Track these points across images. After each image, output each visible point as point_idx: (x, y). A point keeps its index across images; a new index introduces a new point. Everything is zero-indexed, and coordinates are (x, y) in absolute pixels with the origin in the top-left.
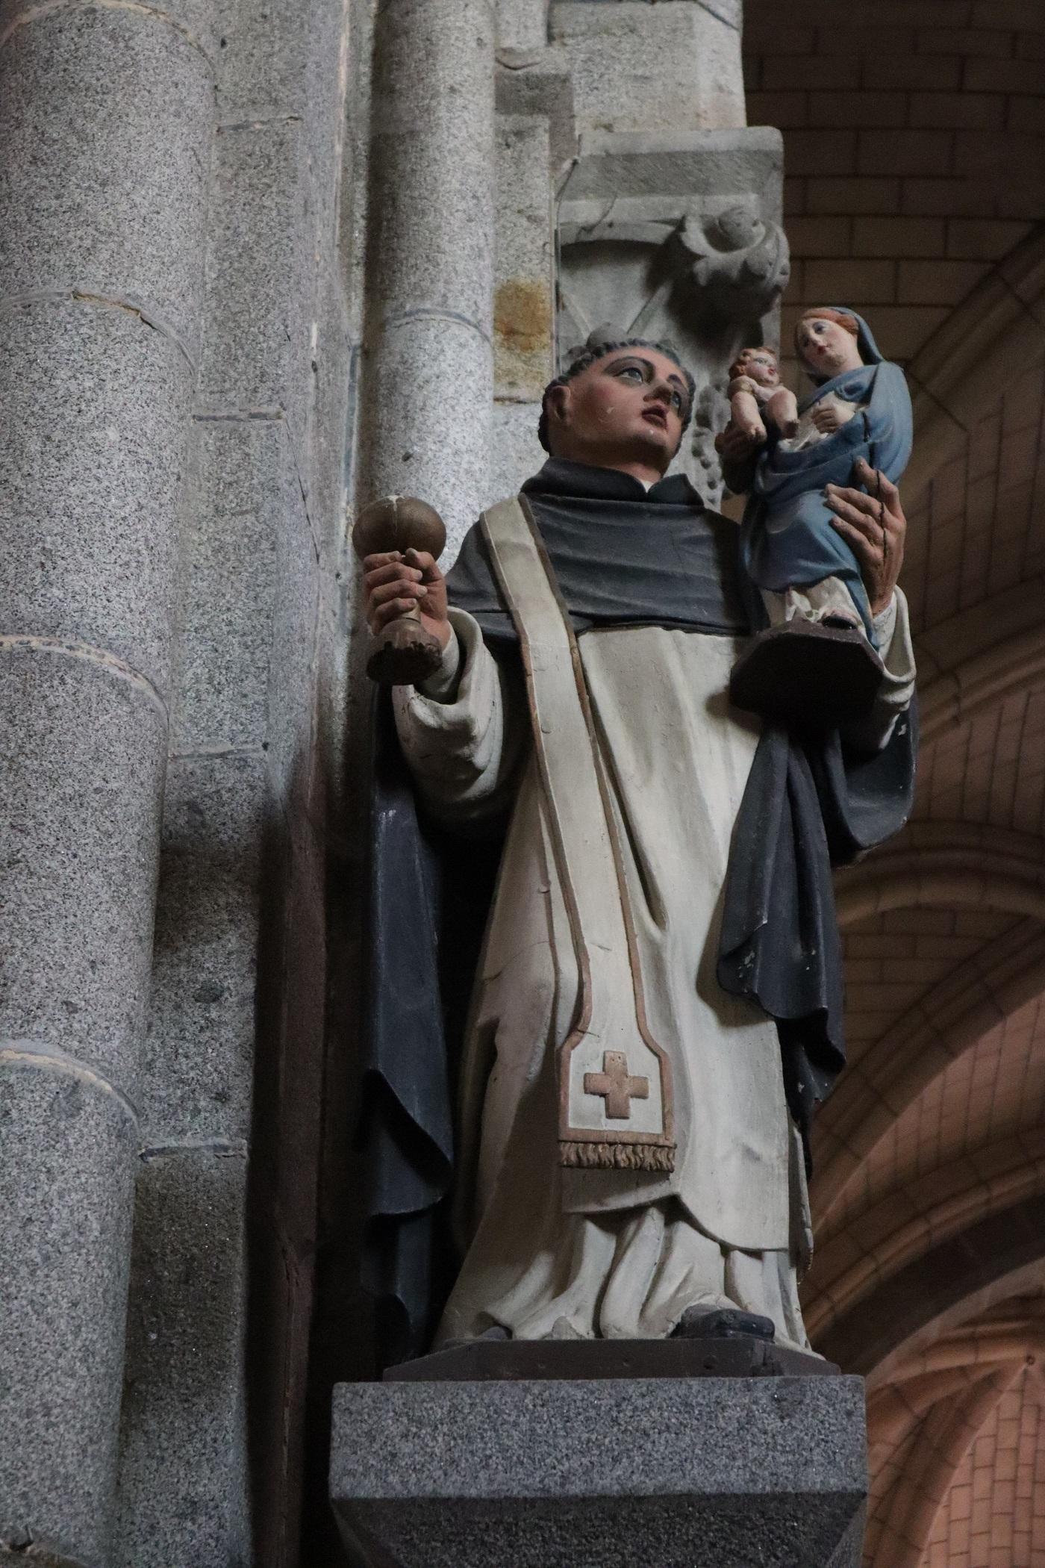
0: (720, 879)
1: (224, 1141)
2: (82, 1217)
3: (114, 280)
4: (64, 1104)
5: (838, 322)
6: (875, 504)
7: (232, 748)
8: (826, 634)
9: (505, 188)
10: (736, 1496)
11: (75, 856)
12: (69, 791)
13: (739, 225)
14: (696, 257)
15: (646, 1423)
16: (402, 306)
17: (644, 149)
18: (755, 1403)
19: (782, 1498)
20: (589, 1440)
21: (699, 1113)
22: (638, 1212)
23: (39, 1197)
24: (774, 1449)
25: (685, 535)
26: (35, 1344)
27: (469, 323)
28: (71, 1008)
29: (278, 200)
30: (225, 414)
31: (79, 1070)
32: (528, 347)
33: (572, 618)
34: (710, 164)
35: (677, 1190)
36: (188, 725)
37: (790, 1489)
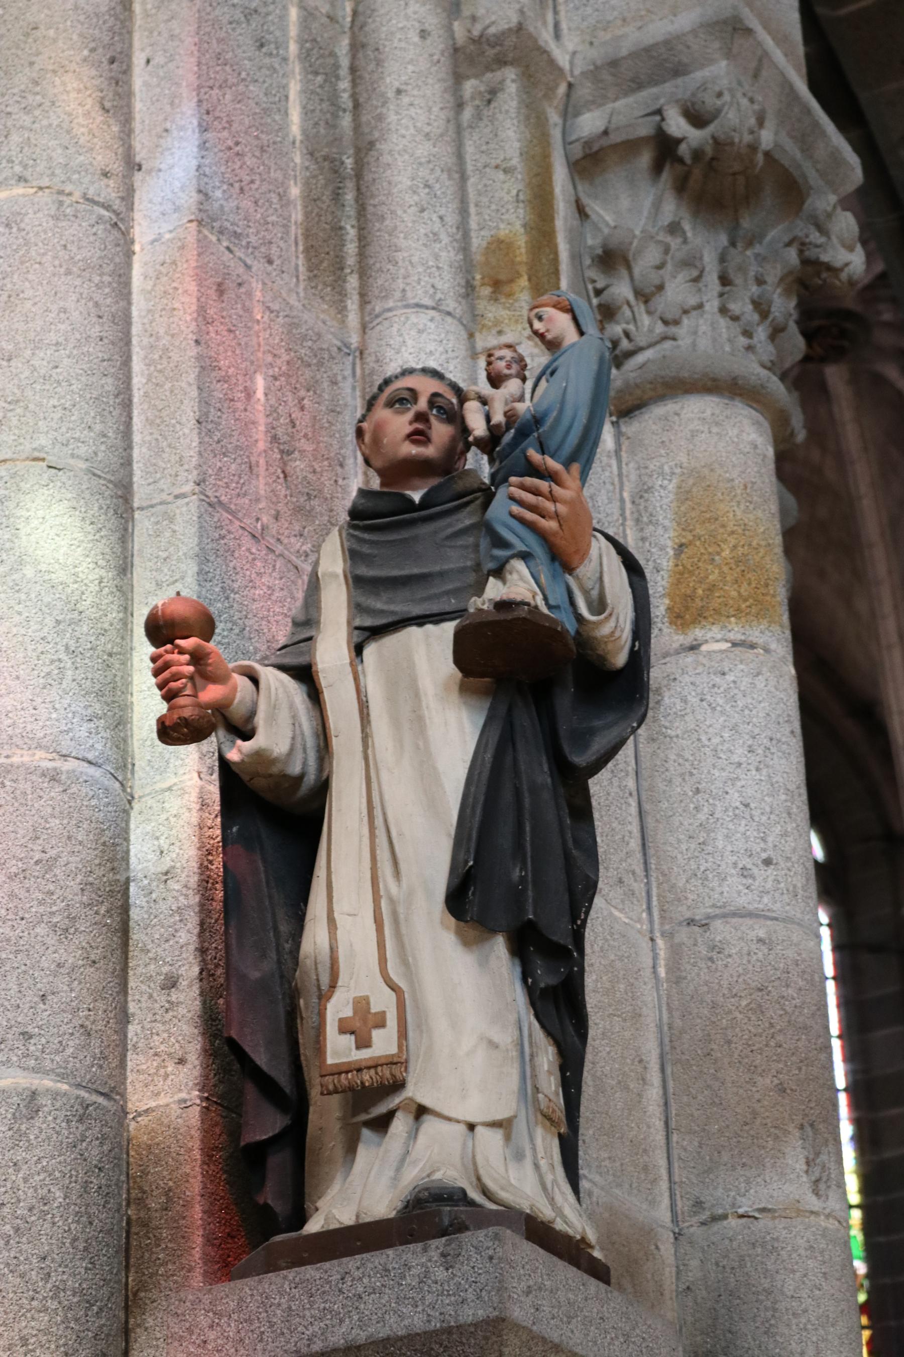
0: (453, 832)
1: (183, 1095)
2: (45, 1191)
3: (22, 440)
4: (24, 1111)
5: (554, 306)
6: (543, 485)
7: (176, 780)
8: (502, 616)
9: (484, 148)
10: (418, 1334)
11: (22, 919)
12: (14, 870)
13: (703, 102)
14: (679, 141)
15: (360, 1289)
16: (374, 310)
17: (624, 52)
18: (430, 1260)
19: (449, 1331)
20: (324, 1309)
21: (440, 1025)
22: (389, 1116)
23: (9, 1185)
24: (442, 1294)
25: (450, 531)
26: (11, 1295)
27: (427, 308)
28: (27, 1036)
29: (183, 300)
30: (158, 501)
31: (36, 1082)
32: (509, 295)
33: (356, 632)
34: (680, 47)
35: (410, 1094)
36: (148, 768)
37: (452, 1324)
